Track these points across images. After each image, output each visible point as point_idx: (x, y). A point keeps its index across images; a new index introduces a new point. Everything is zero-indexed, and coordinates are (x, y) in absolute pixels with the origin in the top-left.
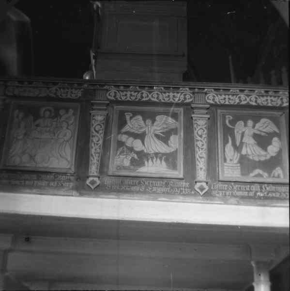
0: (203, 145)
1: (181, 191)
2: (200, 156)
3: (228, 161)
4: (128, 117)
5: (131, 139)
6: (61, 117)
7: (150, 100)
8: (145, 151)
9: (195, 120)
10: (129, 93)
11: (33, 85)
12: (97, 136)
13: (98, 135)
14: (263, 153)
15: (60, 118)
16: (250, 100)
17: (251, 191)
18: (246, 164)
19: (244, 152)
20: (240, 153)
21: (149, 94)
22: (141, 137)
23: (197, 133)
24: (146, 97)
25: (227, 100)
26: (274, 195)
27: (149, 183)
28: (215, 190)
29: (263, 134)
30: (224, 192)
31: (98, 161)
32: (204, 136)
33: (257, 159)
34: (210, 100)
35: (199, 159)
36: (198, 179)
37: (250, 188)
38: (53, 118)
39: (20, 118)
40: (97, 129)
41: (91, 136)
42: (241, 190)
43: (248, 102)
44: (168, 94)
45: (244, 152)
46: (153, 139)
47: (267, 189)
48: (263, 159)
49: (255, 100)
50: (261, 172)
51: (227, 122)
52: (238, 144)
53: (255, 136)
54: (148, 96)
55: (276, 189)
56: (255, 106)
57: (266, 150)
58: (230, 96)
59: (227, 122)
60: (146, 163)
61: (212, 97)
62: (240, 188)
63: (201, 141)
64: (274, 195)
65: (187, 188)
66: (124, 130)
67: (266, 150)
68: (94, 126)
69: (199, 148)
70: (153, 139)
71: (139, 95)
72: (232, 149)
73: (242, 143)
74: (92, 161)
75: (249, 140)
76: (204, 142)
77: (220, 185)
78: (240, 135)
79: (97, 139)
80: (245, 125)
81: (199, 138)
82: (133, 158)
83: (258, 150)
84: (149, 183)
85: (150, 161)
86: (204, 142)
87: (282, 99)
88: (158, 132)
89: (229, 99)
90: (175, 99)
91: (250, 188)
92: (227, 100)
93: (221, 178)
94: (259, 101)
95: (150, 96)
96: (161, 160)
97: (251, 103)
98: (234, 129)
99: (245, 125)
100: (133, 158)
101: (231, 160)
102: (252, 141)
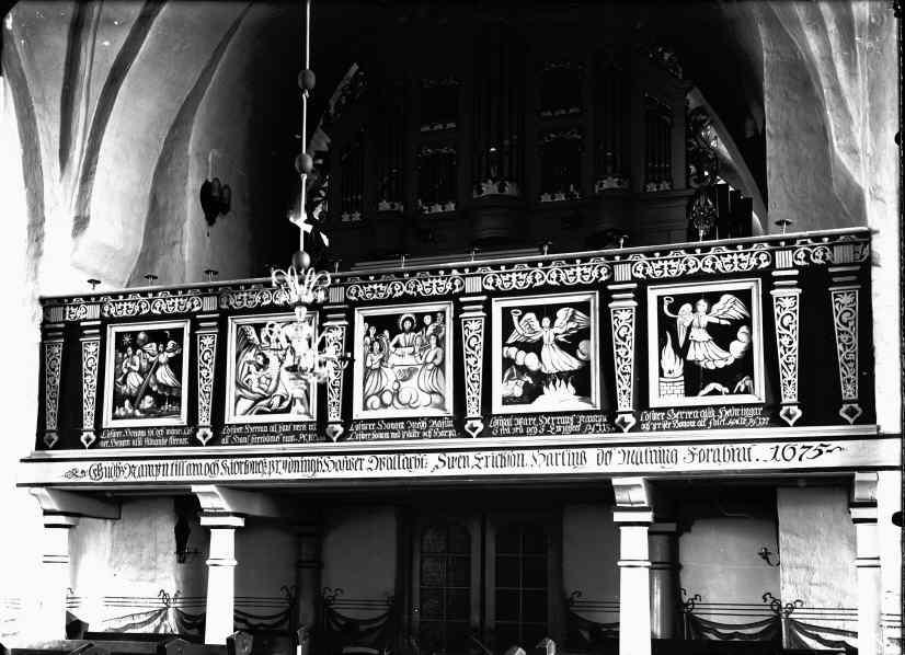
0: (791, 343)
5: (522, 353)
6: (427, 327)
7: (405, 293)
8: (543, 370)
10: (514, 276)
11: (668, 257)
12: (624, 346)
13: (626, 344)
14: (724, 354)
16: (704, 266)
17: (700, 419)
18: (695, 378)
19: (690, 357)
20: (685, 361)
27: (550, 421)
29: (723, 322)
33: (711, 366)
35: (471, 384)
39: (372, 336)
40: (622, 335)
43: (405, 293)
44: (573, 270)
45: (690, 357)
47: (727, 413)
48: (721, 365)
49: (822, 254)
50: (719, 387)
56: (711, 273)
58: (671, 262)
59: (665, 308)
62: (684, 415)
63: (624, 346)
66: (510, 341)
71: (530, 277)
72: (672, 352)
73: (687, 343)
74: (784, 377)
75: (700, 335)
77: (656, 416)
79: (788, 340)
80: (694, 311)
81: (621, 342)
82: (527, 382)
85: (551, 385)
87: (686, 262)
89: (669, 266)
93: (651, 406)
94: (718, 266)
97: (550, 282)
99: (694, 311)
102: (706, 336)
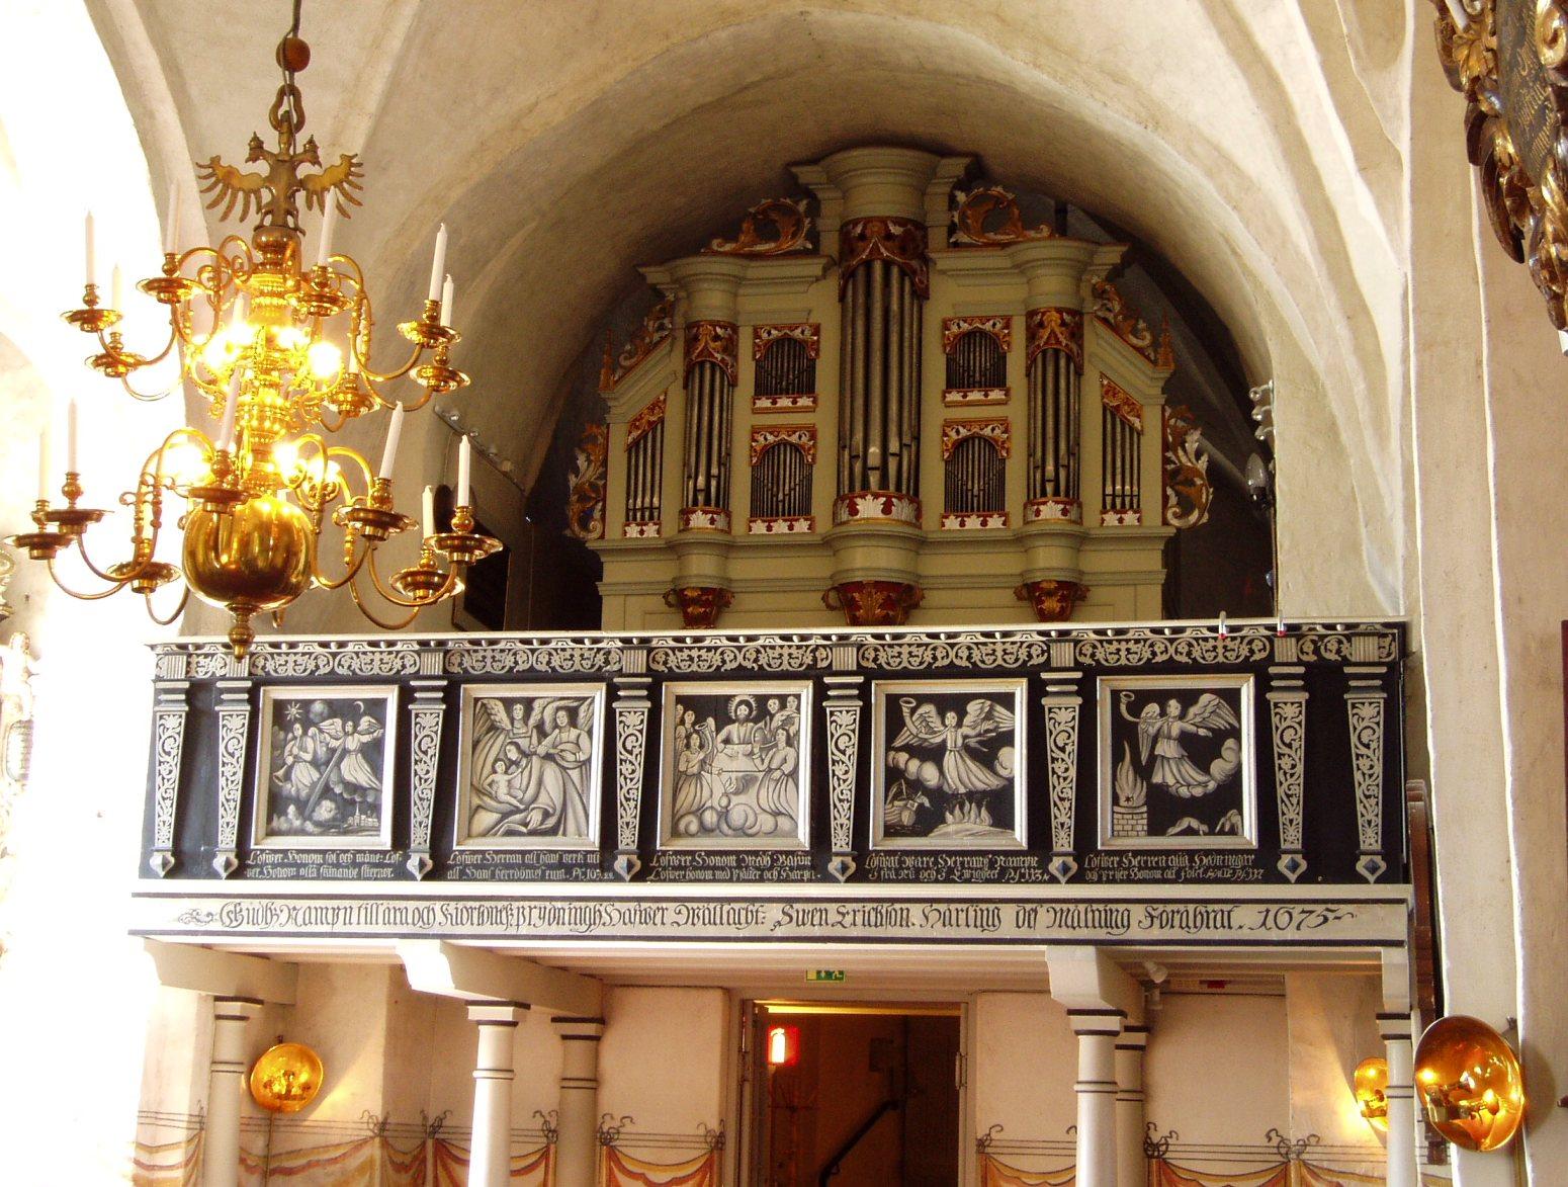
1: (1022, 876)
2: (1367, 793)
3: (1122, 802)
4: (906, 711)
6: (772, 716)
9: (1354, 706)
15: (771, 720)
16: (1176, 652)
17: (1168, 867)
19: (1157, 779)
21: (949, 649)
22: (934, 754)
23: (226, 747)
24: (1260, 651)
25: (1123, 653)
26: (1219, 874)
27: (955, 862)
28: (1091, 869)
30: (1111, 873)
31: (849, 819)
32: (1069, 749)
34: (1181, 654)
36: (1057, 848)
37: (1167, 861)
38: (756, 721)
39: (688, 725)
41: (1276, 755)
42: (1146, 868)
45: (1157, 779)
46: (964, 761)
47: (1205, 861)
48: (1198, 792)
50: (1195, 824)
51: (1123, 708)
52: (1144, 757)
53: (1185, 739)
54: (1166, 651)
55: (1224, 860)
57: (1206, 770)
59: (1123, 708)
60: (948, 815)
61: (1187, 649)
64: (1219, 874)
65: (1034, 868)
67: (1206, 770)
68: (1357, 732)
69: (1059, 777)
70: (964, 761)
76: (636, 764)
78: (1150, 740)
82: (921, 805)
83: (1191, 772)
84: (955, 862)
86: (1375, 759)
88: (972, 742)
90: (1227, 654)
91: (1167, 861)
92: (1123, 653)
95: (1171, 650)
96: (979, 807)
98: (1137, 724)
100: (921, 805)
101: (1128, 799)
